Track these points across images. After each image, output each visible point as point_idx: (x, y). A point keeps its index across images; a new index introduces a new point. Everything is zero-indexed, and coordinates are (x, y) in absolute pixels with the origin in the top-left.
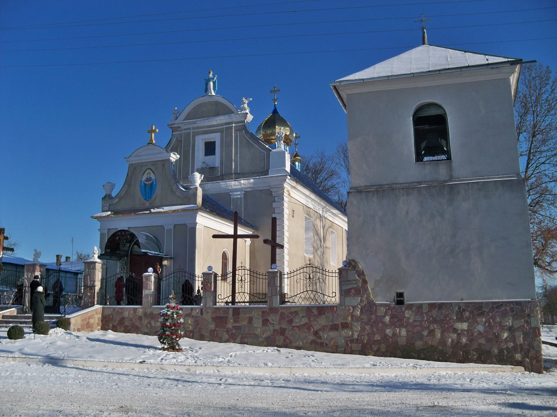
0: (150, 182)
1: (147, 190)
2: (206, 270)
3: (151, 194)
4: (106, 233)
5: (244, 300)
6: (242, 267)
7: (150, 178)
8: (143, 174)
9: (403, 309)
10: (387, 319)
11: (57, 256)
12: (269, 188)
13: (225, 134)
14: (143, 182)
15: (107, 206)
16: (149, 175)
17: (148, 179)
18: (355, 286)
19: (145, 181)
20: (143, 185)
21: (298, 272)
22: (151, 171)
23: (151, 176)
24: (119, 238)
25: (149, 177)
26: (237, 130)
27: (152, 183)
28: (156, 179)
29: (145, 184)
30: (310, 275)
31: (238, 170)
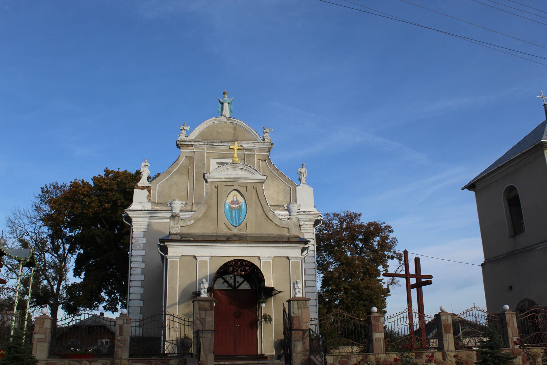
0: (237, 206)
1: (234, 214)
4: (177, 261)
6: (475, 307)
7: (238, 201)
11: (401, 285)
14: (227, 204)
15: (177, 227)
16: (235, 197)
17: (233, 202)
22: (238, 193)
23: (238, 199)
24: (234, 269)
25: (235, 200)
29: (230, 207)
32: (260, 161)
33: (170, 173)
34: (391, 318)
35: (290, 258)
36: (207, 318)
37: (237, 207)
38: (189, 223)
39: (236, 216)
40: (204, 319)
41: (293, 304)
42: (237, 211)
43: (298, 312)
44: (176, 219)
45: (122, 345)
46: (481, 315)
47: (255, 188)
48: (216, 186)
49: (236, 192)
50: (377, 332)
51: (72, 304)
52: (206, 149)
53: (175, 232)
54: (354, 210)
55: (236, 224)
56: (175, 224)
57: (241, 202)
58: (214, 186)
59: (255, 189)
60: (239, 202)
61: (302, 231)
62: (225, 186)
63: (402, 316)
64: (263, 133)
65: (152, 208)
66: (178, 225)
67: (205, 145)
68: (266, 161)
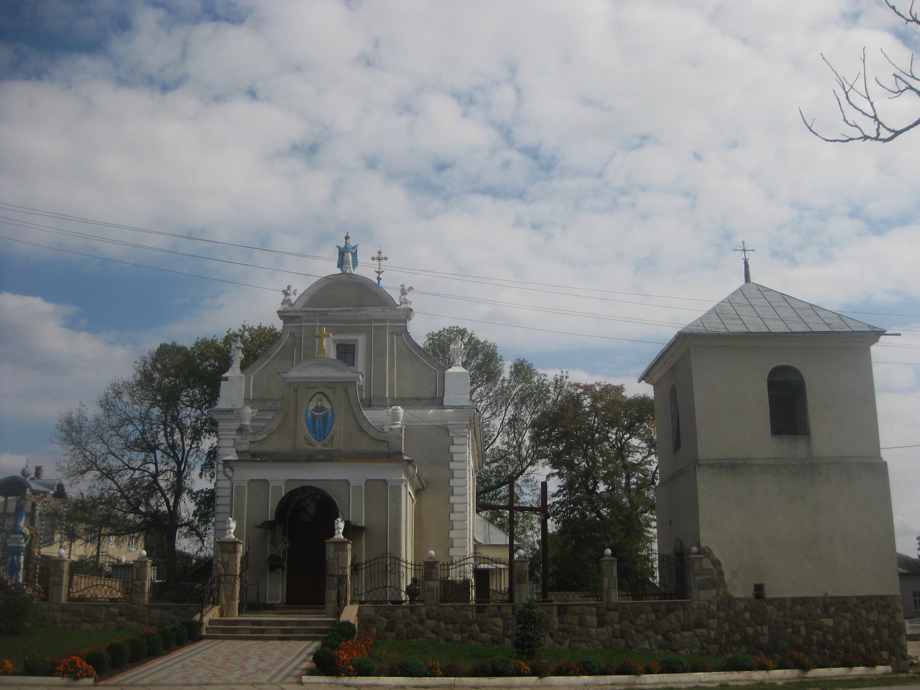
0: (321, 414)
3: (325, 431)
5: (396, 591)
8: (310, 400)
9: (765, 604)
10: (747, 615)
12: (444, 423)
13: (374, 336)
15: (245, 443)
16: (320, 403)
17: (317, 409)
18: (709, 576)
19: (312, 410)
23: (324, 405)
25: (320, 405)
26: (393, 333)
28: (332, 409)
29: (313, 416)
34: (460, 561)
35: (388, 481)
42: (321, 420)
45: (139, 590)
46: (395, 564)
47: (346, 389)
48: (296, 388)
51: (482, 501)
52: (318, 321)
54: (615, 382)
55: (320, 437)
56: (242, 440)
58: (292, 388)
59: (346, 391)
60: (324, 408)
61: (451, 434)
63: (376, 561)
64: (407, 287)
66: (247, 441)
68: (403, 334)
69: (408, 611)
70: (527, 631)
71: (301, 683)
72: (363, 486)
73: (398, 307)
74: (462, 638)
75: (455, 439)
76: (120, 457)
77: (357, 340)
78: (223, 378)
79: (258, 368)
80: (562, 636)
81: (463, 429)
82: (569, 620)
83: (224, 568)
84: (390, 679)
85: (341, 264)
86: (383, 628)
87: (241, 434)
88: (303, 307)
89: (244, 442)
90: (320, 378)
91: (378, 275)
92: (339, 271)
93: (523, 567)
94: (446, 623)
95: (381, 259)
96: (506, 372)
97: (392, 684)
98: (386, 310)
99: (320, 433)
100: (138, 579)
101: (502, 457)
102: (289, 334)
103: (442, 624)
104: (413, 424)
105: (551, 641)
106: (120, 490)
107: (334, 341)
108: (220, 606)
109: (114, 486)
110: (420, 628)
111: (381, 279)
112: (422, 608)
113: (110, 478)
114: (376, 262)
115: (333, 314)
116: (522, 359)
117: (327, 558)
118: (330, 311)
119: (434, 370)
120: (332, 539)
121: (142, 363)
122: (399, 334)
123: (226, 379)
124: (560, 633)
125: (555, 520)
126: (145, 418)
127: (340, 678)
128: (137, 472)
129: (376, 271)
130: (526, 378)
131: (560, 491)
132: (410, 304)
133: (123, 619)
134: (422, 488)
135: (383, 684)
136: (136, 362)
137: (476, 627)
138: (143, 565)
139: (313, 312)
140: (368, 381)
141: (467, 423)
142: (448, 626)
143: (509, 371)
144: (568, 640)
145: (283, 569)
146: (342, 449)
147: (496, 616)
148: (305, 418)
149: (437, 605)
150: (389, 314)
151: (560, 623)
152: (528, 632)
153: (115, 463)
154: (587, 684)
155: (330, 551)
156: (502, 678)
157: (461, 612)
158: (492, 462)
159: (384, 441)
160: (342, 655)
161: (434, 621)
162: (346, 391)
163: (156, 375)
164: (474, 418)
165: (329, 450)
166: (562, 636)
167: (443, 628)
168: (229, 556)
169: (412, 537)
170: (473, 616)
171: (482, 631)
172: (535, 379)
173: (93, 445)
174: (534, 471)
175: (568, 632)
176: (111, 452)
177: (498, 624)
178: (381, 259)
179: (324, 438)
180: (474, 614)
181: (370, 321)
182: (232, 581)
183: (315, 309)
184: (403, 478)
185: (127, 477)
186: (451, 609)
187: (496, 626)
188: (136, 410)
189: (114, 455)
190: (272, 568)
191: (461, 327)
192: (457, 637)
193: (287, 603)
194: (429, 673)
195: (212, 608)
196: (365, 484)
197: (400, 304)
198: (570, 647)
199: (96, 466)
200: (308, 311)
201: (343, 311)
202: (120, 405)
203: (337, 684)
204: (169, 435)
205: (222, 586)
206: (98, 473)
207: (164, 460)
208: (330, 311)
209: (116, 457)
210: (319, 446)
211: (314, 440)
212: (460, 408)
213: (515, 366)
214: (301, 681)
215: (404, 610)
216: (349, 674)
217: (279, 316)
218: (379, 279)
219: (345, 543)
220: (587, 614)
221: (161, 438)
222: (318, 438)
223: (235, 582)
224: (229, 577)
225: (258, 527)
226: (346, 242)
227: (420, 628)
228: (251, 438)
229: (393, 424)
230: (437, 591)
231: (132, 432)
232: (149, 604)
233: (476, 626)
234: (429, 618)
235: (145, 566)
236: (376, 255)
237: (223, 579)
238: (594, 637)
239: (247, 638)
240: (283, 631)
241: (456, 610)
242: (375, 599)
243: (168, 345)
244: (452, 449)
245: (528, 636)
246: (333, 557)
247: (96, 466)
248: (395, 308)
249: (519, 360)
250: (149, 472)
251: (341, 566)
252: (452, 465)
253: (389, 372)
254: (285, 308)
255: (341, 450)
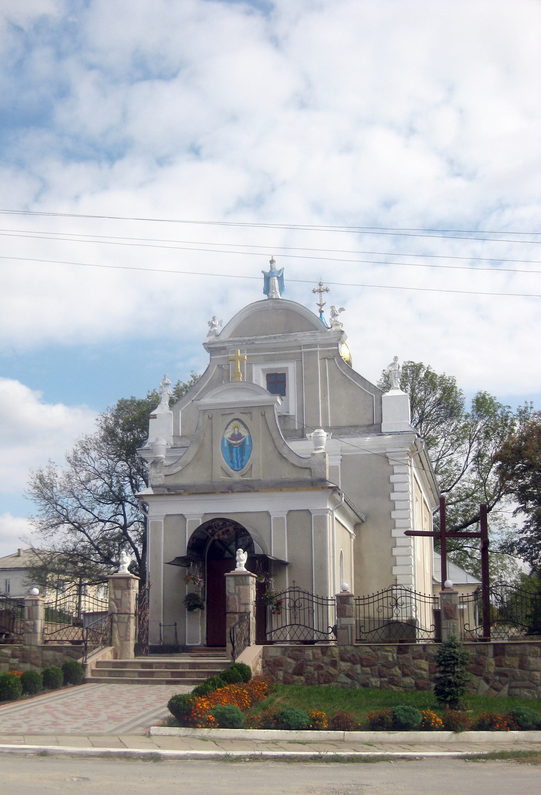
0: (239, 442)
2: (338, 592)
3: (242, 460)
8: (226, 428)
12: (385, 451)
16: (236, 430)
17: (233, 437)
19: (229, 438)
20: (226, 444)
21: (380, 596)
22: (240, 424)
23: (240, 432)
25: (236, 433)
26: (324, 358)
27: (244, 443)
28: (250, 436)
29: (230, 444)
30: (295, 603)
31: (328, 423)
32: (325, 361)
33: (197, 392)
36: (123, 598)
37: (240, 443)
38: (176, 469)
39: (237, 457)
40: (120, 600)
41: (229, 581)
42: (239, 448)
43: (235, 591)
44: (159, 466)
45: (31, 631)
47: (263, 414)
49: (237, 422)
50: (343, 617)
53: (158, 484)
55: (238, 467)
57: (244, 436)
58: (207, 416)
59: (263, 415)
61: (391, 463)
62: (222, 415)
65: (175, 444)
66: (161, 474)
67: (242, 345)
69: (319, 651)
70: (448, 674)
71: (149, 735)
72: (285, 517)
73: (329, 330)
74: (381, 682)
75: (395, 467)
76: (90, 510)
77: (287, 368)
78: (152, 416)
79: (185, 405)
80: (500, 681)
81: (403, 456)
82: (508, 663)
83: (117, 606)
84: (262, 732)
85: (267, 290)
86: (290, 671)
87: (155, 467)
88: (230, 337)
89: (159, 475)
90: (236, 403)
91: (320, 307)
92: (265, 297)
93: (451, 600)
94: (363, 666)
95: (322, 291)
96: (468, 408)
97: (263, 738)
98: (316, 334)
99: (238, 462)
100: (30, 619)
101: (468, 496)
102: (216, 366)
103: (358, 667)
104: (350, 454)
105: (487, 687)
106: (92, 542)
107: (263, 370)
108: (113, 647)
109: (86, 539)
110: (332, 670)
111: (323, 312)
112: (335, 648)
113: (81, 531)
114: (317, 295)
115: (260, 342)
116: (483, 392)
117: (227, 594)
118: (257, 340)
119: (370, 395)
120: (232, 572)
121: (103, 420)
122: (331, 359)
123: (155, 417)
124: (497, 678)
125: (522, 557)
126: (110, 472)
127: (198, 730)
128: (108, 524)
129: (317, 304)
130: (488, 411)
131: (527, 527)
132: (342, 326)
133: (16, 661)
134: (360, 522)
135: (251, 738)
136: (97, 420)
137: (397, 671)
138: (34, 604)
139: (239, 341)
140: (301, 409)
141: (408, 449)
142: (364, 668)
143: (471, 406)
144: (507, 686)
145: (203, 609)
146: (261, 478)
147: (421, 658)
148: (222, 448)
149: (352, 645)
150: (320, 338)
151: (497, 666)
152: (450, 676)
153: (86, 516)
154: (516, 741)
155: (230, 585)
156: (405, 732)
157: (379, 653)
158: (457, 501)
159: (306, 468)
160: (202, 702)
161: (349, 664)
162: (263, 415)
163: (119, 430)
164: (415, 444)
165: (247, 480)
166: (500, 681)
167: (359, 671)
168: (122, 592)
169: (351, 574)
170: (393, 658)
171: (405, 675)
172: (499, 412)
173: (65, 500)
174: (501, 509)
175: (506, 676)
176: (82, 505)
177: (422, 666)
178: (322, 291)
179: (243, 468)
180: (395, 655)
181: (300, 347)
182: (126, 620)
183: (242, 339)
184: (328, 507)
185: (98, 529)
186: (368, 650)
187: (421, 669)
188: (101, 464)
189: (84, 508)
190: (191, 608)
191: (417, 362)
192: (375, 681)
193: (208, 645)
194: (311, 726)
195: (102, 649)
196: (287, 515)
197: (330, 327)
198: (509, 694)
199: (68, 520)
200: (235, 341)
201: (270, 338)
202: (89, 461)
203: (194, 737)
204: (135, 487)
205: (115, 625)
206: (71, 526)
207: (133, 512)
208: (257, 340)
209: (87, 510)
210: (237, 477)
211: (232, 471)
212: (399, 434)
213: (477, 401)
214: (149, 733)
215: (314, 651)
216: (208, 725)
217: (205, 348)
218: (321, 312)
219: (246, 576)
220: (530, 655)
221: (128, 489)
222: (236, 468)
223: (129, 621)
224: (123, 616)
225: (169, 563)
226: (271, 266)
227: (332, 670)
228: (166, 471)
229: (315, 450)
230: (352, 630)
231: (99, 485)
232: (43, 645)
233: (397, 669)
234: (343, 659)
235: (37, 605)
236: (317, 287)
237: (116, 617)
238: (539, 682)
239: (133, 682)
240: (173, 674)
241: (374, 651)
242: (302, 638)
243: (127, 401)
244: (393, 479)
245: (450, 682)
246: (234, 592)
247: (68, 520)
248: (325, 332)
249: (480, 393)
250: (118, 524)
251: (242, 602)
252: (393, 496)
253: (322, 399)
254: (211, 340)
255: (260, 480)
